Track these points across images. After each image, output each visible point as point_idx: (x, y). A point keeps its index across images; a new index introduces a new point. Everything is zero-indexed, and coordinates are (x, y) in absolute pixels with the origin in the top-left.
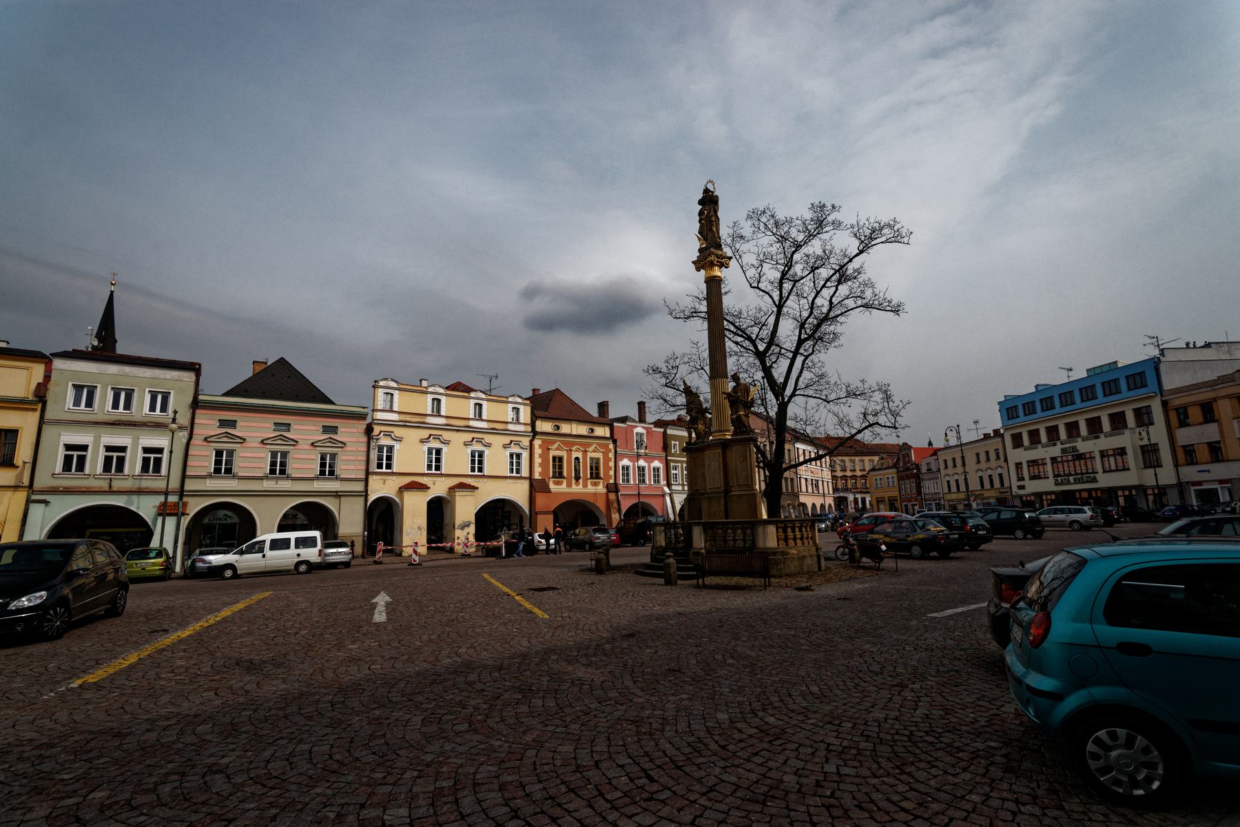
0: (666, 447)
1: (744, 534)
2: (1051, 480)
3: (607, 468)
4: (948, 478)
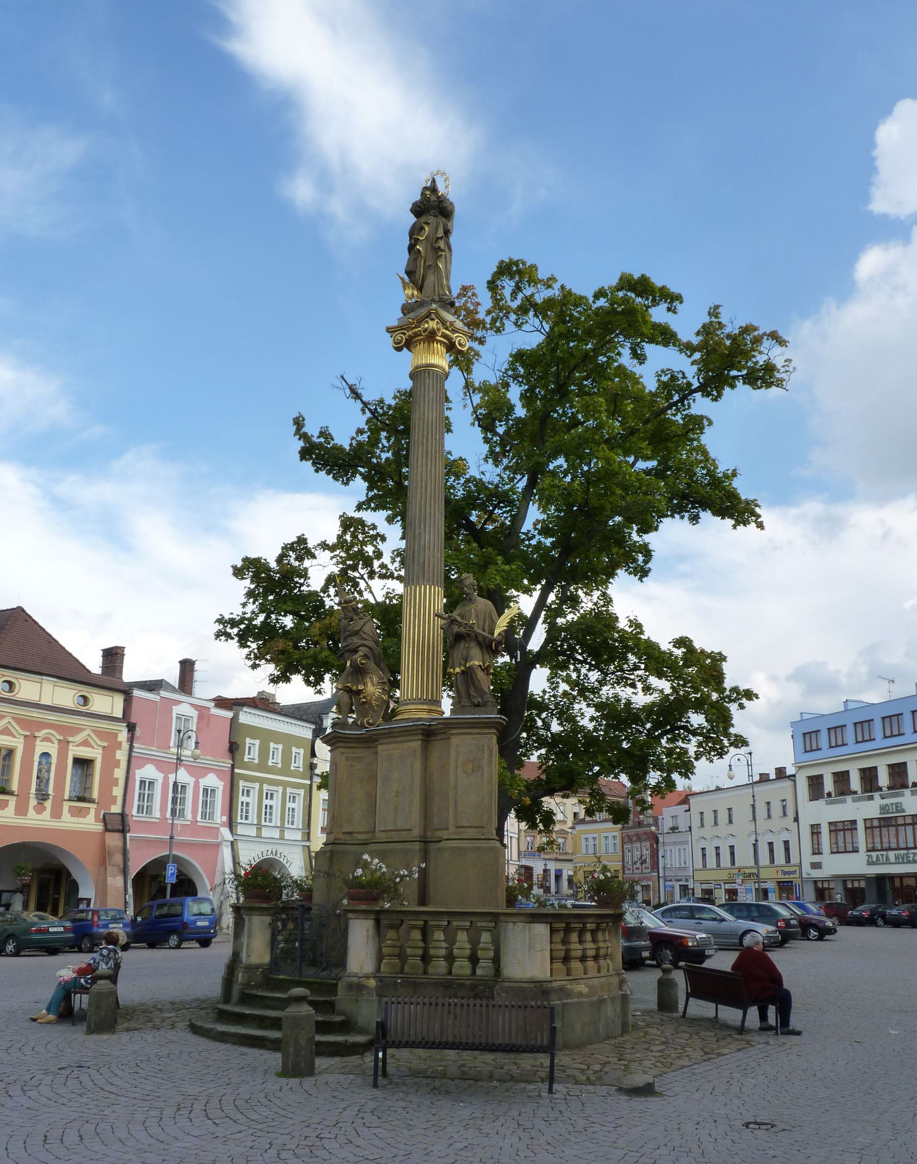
0: (234, 749)
1: (474, 942)
2: (862, 855)
3: (108, 781)
4: (703, 844)
